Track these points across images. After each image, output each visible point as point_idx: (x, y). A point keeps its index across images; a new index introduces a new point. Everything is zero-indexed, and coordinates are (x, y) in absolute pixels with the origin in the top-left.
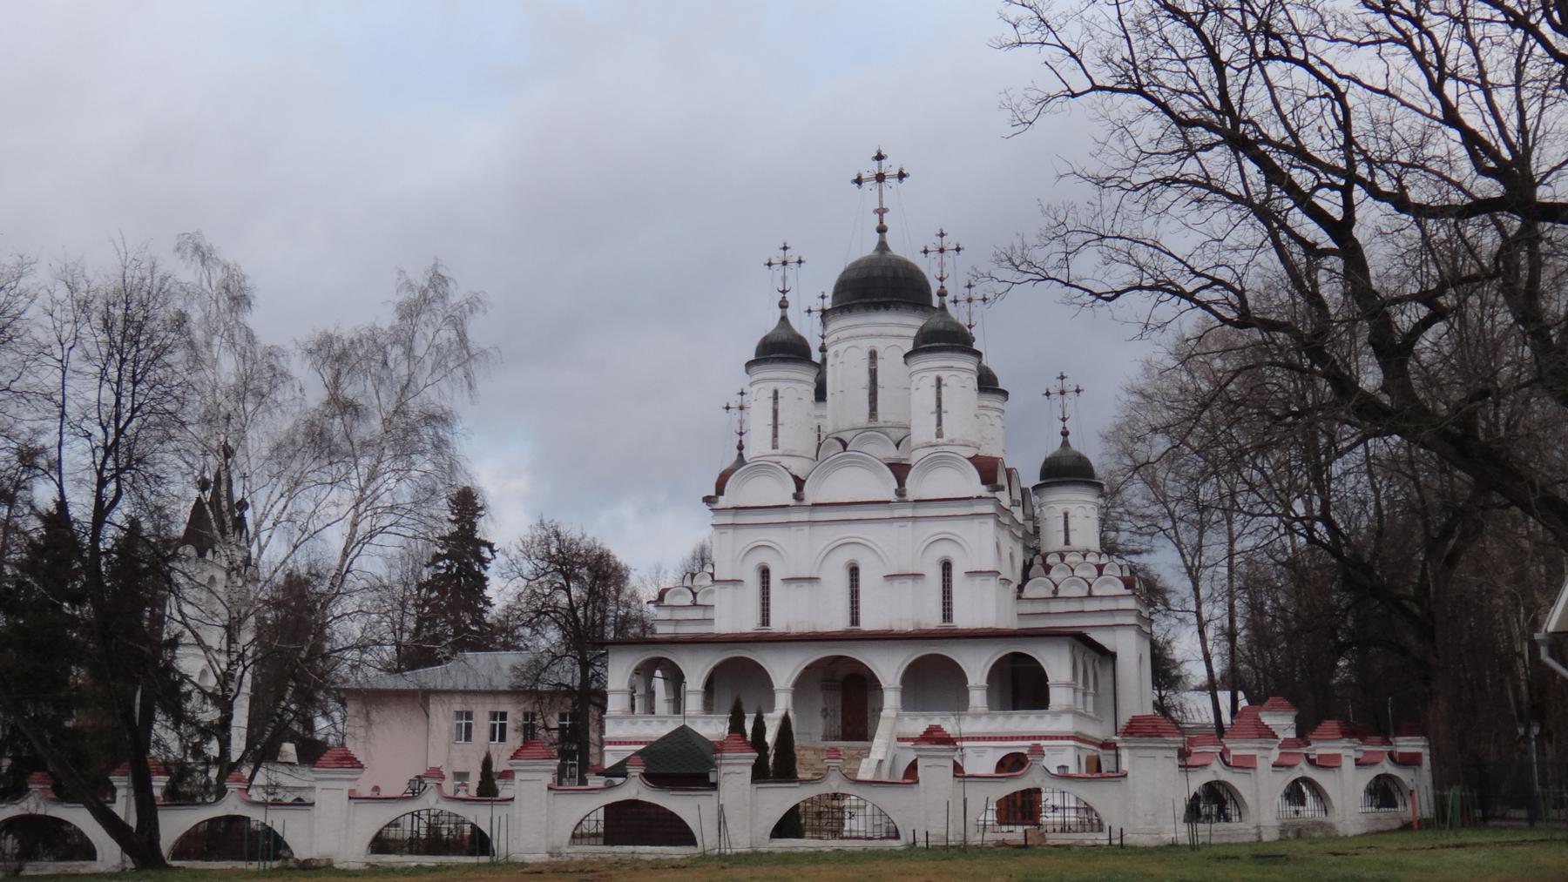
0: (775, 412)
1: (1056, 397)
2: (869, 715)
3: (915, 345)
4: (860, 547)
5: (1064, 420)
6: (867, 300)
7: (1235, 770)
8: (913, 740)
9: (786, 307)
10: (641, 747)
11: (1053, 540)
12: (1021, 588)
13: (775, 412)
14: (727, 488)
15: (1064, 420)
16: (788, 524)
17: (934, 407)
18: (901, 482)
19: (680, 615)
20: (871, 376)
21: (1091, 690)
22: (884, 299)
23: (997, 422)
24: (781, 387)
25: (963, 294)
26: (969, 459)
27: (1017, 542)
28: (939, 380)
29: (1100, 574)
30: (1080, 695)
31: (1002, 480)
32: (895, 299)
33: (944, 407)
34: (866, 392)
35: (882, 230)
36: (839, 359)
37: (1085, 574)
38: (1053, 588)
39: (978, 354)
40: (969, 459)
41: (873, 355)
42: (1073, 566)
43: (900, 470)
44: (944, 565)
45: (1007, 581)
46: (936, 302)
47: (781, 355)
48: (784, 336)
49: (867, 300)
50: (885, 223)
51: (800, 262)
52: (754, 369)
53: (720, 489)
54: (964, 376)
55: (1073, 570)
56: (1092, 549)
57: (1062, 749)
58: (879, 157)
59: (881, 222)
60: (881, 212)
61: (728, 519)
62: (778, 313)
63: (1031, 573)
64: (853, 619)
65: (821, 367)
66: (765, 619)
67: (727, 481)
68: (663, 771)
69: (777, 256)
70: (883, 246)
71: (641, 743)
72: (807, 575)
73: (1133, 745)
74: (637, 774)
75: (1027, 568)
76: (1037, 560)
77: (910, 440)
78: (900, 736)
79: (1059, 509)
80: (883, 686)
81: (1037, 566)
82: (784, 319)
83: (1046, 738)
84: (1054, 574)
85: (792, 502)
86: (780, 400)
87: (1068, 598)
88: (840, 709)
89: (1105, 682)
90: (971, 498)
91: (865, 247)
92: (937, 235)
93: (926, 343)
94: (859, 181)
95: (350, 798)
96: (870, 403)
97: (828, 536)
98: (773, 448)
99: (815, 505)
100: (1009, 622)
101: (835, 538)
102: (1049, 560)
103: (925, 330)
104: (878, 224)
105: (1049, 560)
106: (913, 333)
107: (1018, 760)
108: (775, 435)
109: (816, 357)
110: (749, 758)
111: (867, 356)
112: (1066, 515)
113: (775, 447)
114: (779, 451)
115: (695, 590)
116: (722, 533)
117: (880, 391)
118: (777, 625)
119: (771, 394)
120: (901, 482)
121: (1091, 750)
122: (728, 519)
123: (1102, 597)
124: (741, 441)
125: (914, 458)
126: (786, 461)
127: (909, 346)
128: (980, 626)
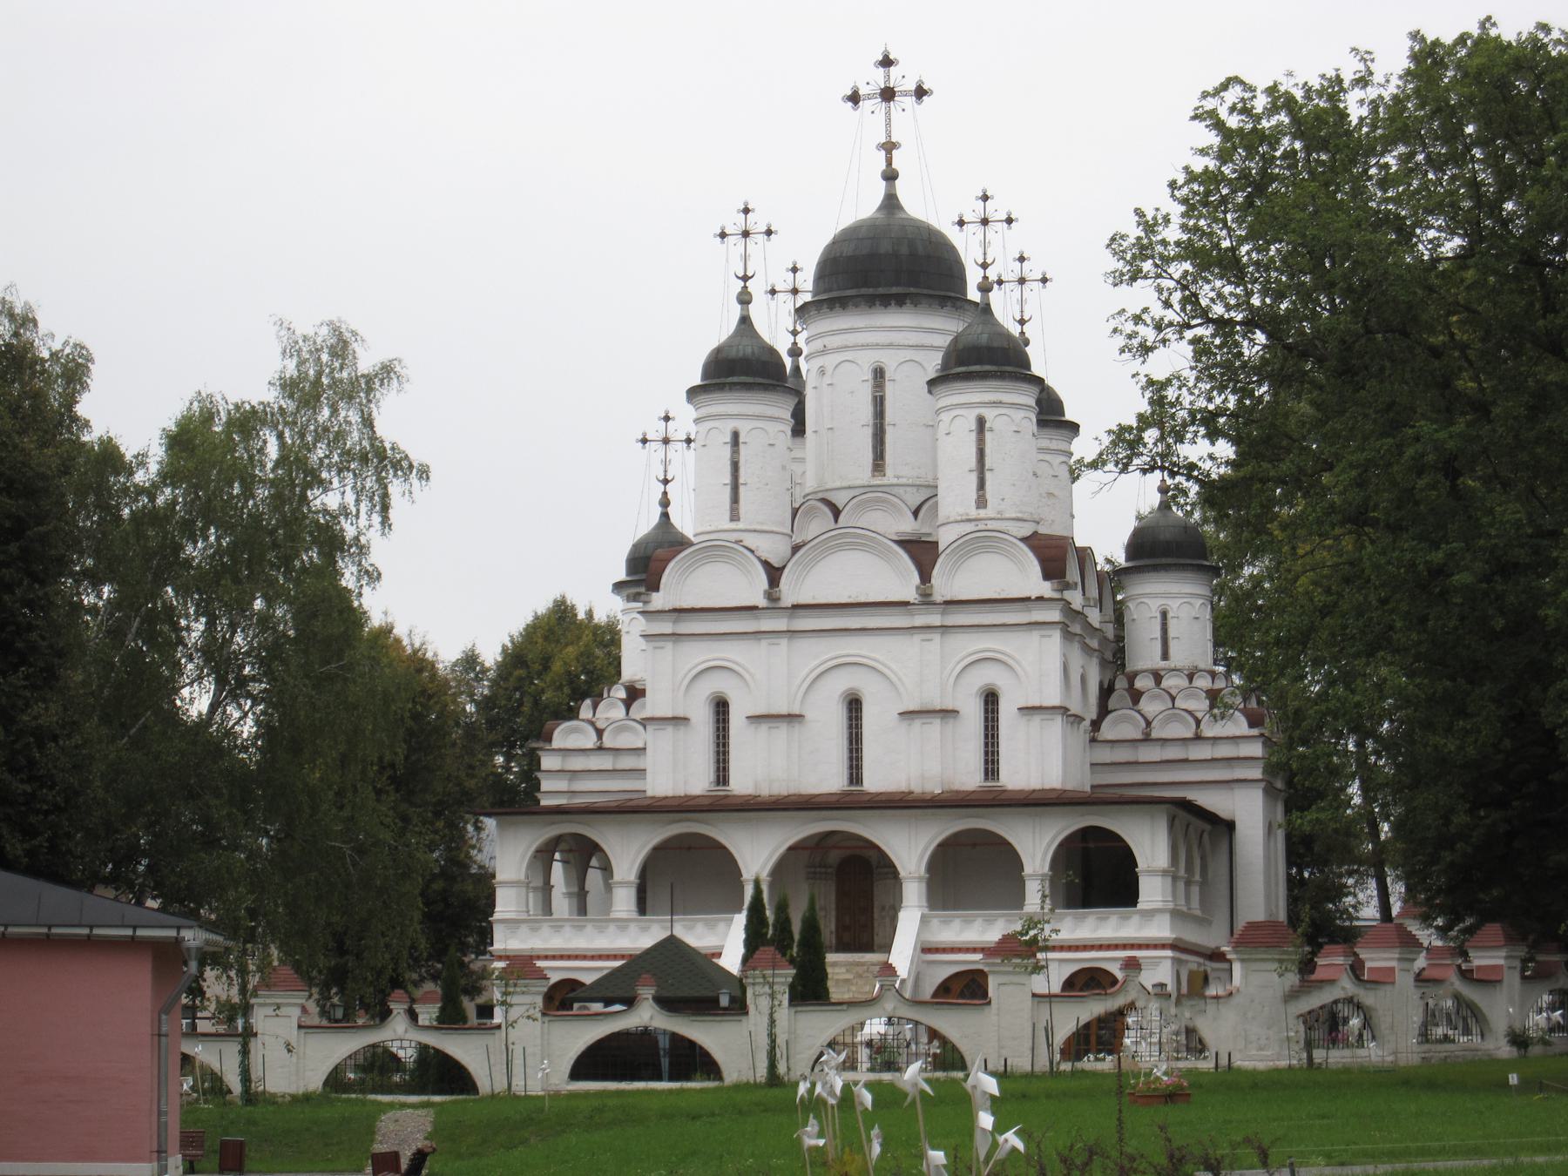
0: (735, 466)
2: (876, 916)
3: (946, 364)
4: (855, 668)
6: (871, 291)
7: (1368, 986)
8: (982, 950)
9: (749, 302)
10: (617, 964)
11: (1144, 654)
12: (1096, 725)
13: (735, 466)
14: (663, 580)
16: (758, 634)
17: (972, 461)
18: (925, 577)
19: (577, 763)
20: (875, 406)
21: (1197, 877)
22: (894, 290)
24: (744, 427)
25: (1010, 270)
26: (1024, 540)
27: (1091, 656)
28: (981, 422)
30: (1181, 885)
31: (1073, 574)
32: (912, 290)
33: (988, 463)
34: (869, 432)
35: (890, 176)
36: (827, 380)
37: (1192, 705)
38: (1143, 724)
39: (1039, 381)
40: (1024, 540)
41: (879, 374)
42: (1174, 692)
43: (922, 552)
44: (987, 696)
45: (1078, 719)
46: (973, 294)
47: (743, 379)
48: (747, 349)
49: (871, 291)
50: (894, 166)
51: (769, 233)
52: (702, 397)
54: (1019, 415)
55: (1173, 699)
56: (1202, 666)
57: (1156, 961)
58: (887, 62)
59: (889, 162)
60: (889, 147)
61: (666, 627)
62: (736, 311)
63: (1111, 704)
64: (851, 774)
65: (798, 394)
66: (722, 775)
67: (667, 564)
68: (696, 995)
69: (735, 223)
70: (891, 202)
71: (615, 957)
72: (784, 711)
73: (1246, 957)
74: (650, 997)
75: (1106, 692)
76: (1121, 683)
77: (936, 506)
78: (924, 946)
79: (1154, 606)
80: (902, 874)
81: (1119, 698)
82: (745, 320)
83: (1147, 947)
85: (761, 602)
86: (742, 447)
87: (1164, 741)
88: (833, 906)
89: (1219, 866)
90: (1028, 599)
91: (865, 205)
92: (977, 198)
93: (961, 364)
94: (854, 98)
95: (300, 1027)
96: (875, 448)
98: (732, 520)
99: (796, 607)
100: (1081, 781)
102: (1140, 683)
103: (960, 346)
104: (883, 166)
105: (1140, 683)
106: (944, 341)
107: (1092, 979)
108: (735, 499)
110: (786, 976)
111: (869, 376)
112: (1164, 615)
113: (735, 516)
114: (740, 525)
116: (655, 648)
117: (889, 430)
118: (741, 784)
119: (728, 439)
120: (925, 577)
121: (1194, 962)
122: (666, 627)
123: (1215, 739)
124: (665, 493)
125: (945, 537)
126: (750, 540)
128: (1038, 786)
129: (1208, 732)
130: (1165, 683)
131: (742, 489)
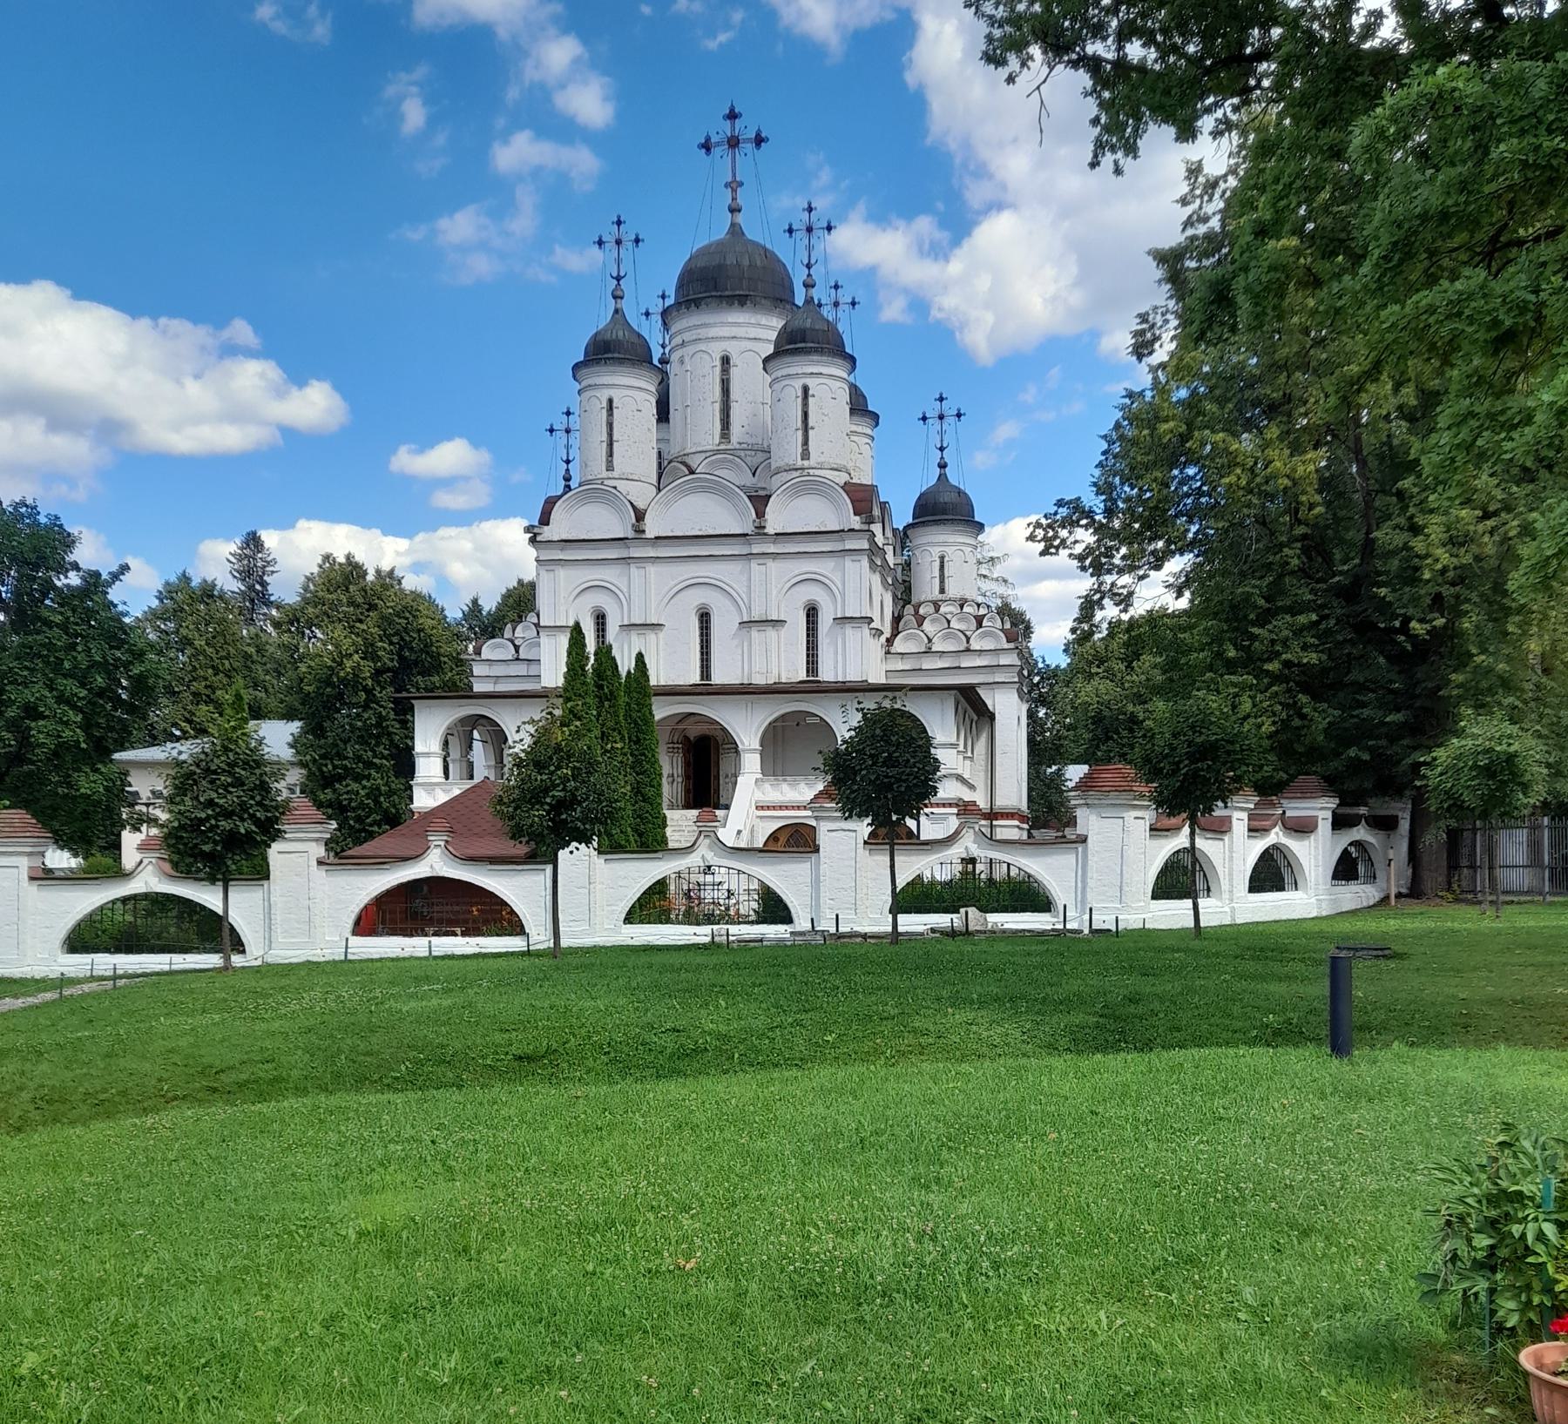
0: (610, 426)
1: (934, 424)
5: (942, 449)
11: (926, 588)
12: (890, 641)
15: (942, 449)
23: (866, 450)
28: (806, 389)
29: (980, 625)
37: (962, 627)
38: (926, 640)
41: (726, 361)
42: (949, 617)
45: (879, 632)
53: (545, 520)
58: (733, 116)
75: (897, 619)
79: (936, 552)
84: (927, 626)
85: (631, 534)
86: (615, 410)
90: (843, 531)
97: (779, 573)
100: (877, 677)
101: (686, 577)
103: (789, 330)
106: (773, 335)
108: (610, 454)
109: (657, 354)
110: (771, 328)
111: (718, 363)
112: (942, 558)
114: (615, 474)
115: (517, 643)
120: (760, 514)
124: (567, 470)
127: (770, 349)
129: (975, 645)
130: (942, 610)
131: (615, 445)
